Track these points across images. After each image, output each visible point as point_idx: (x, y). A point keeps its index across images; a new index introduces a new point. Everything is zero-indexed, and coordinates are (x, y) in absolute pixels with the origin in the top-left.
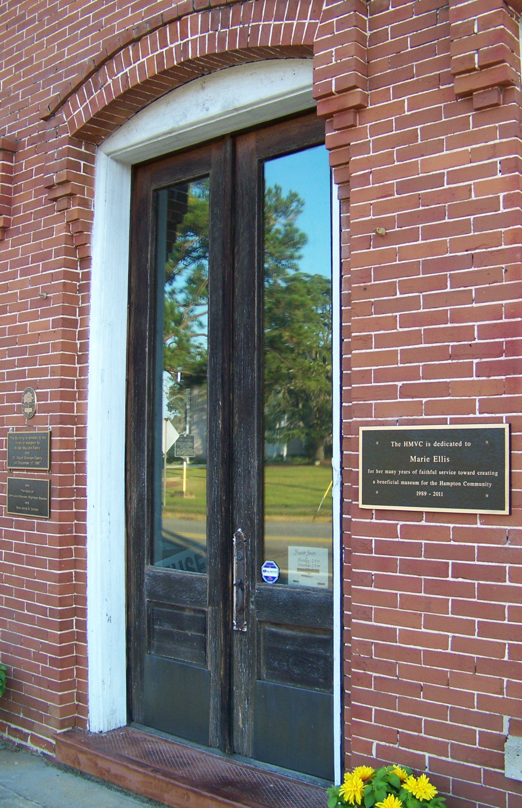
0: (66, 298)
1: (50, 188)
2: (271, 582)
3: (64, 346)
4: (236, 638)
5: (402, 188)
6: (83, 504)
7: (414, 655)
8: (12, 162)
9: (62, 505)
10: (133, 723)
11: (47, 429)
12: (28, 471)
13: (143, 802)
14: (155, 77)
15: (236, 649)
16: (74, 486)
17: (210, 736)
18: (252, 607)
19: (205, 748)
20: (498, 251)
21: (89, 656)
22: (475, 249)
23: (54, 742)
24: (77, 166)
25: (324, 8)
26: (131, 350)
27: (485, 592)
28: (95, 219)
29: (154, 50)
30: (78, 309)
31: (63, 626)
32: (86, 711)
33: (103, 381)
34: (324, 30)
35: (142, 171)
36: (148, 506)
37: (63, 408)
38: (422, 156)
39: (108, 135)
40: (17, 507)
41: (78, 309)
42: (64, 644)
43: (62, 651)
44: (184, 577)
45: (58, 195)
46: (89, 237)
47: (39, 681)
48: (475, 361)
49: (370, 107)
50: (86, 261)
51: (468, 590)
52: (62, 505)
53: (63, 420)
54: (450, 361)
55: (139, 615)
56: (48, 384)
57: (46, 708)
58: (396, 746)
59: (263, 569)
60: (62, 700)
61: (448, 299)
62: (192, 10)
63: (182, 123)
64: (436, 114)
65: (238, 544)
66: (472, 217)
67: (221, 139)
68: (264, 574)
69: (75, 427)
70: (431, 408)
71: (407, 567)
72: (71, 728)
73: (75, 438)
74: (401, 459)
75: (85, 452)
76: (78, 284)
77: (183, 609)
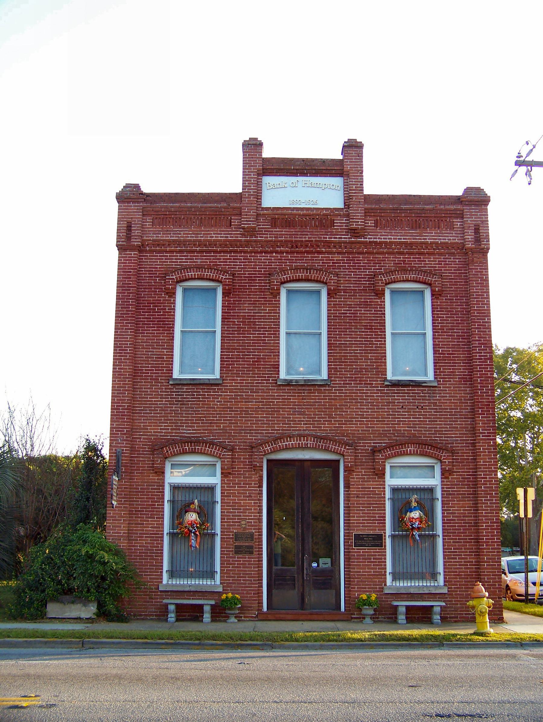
7: (365, 575)
26: (338, 553)
27: (379, 562)
34: (347, 452)
51: (376, 562)
61: (372, 510)
64: (369, 475)
70: (368, 530)
71: (363, 559)
74: (362, 539)
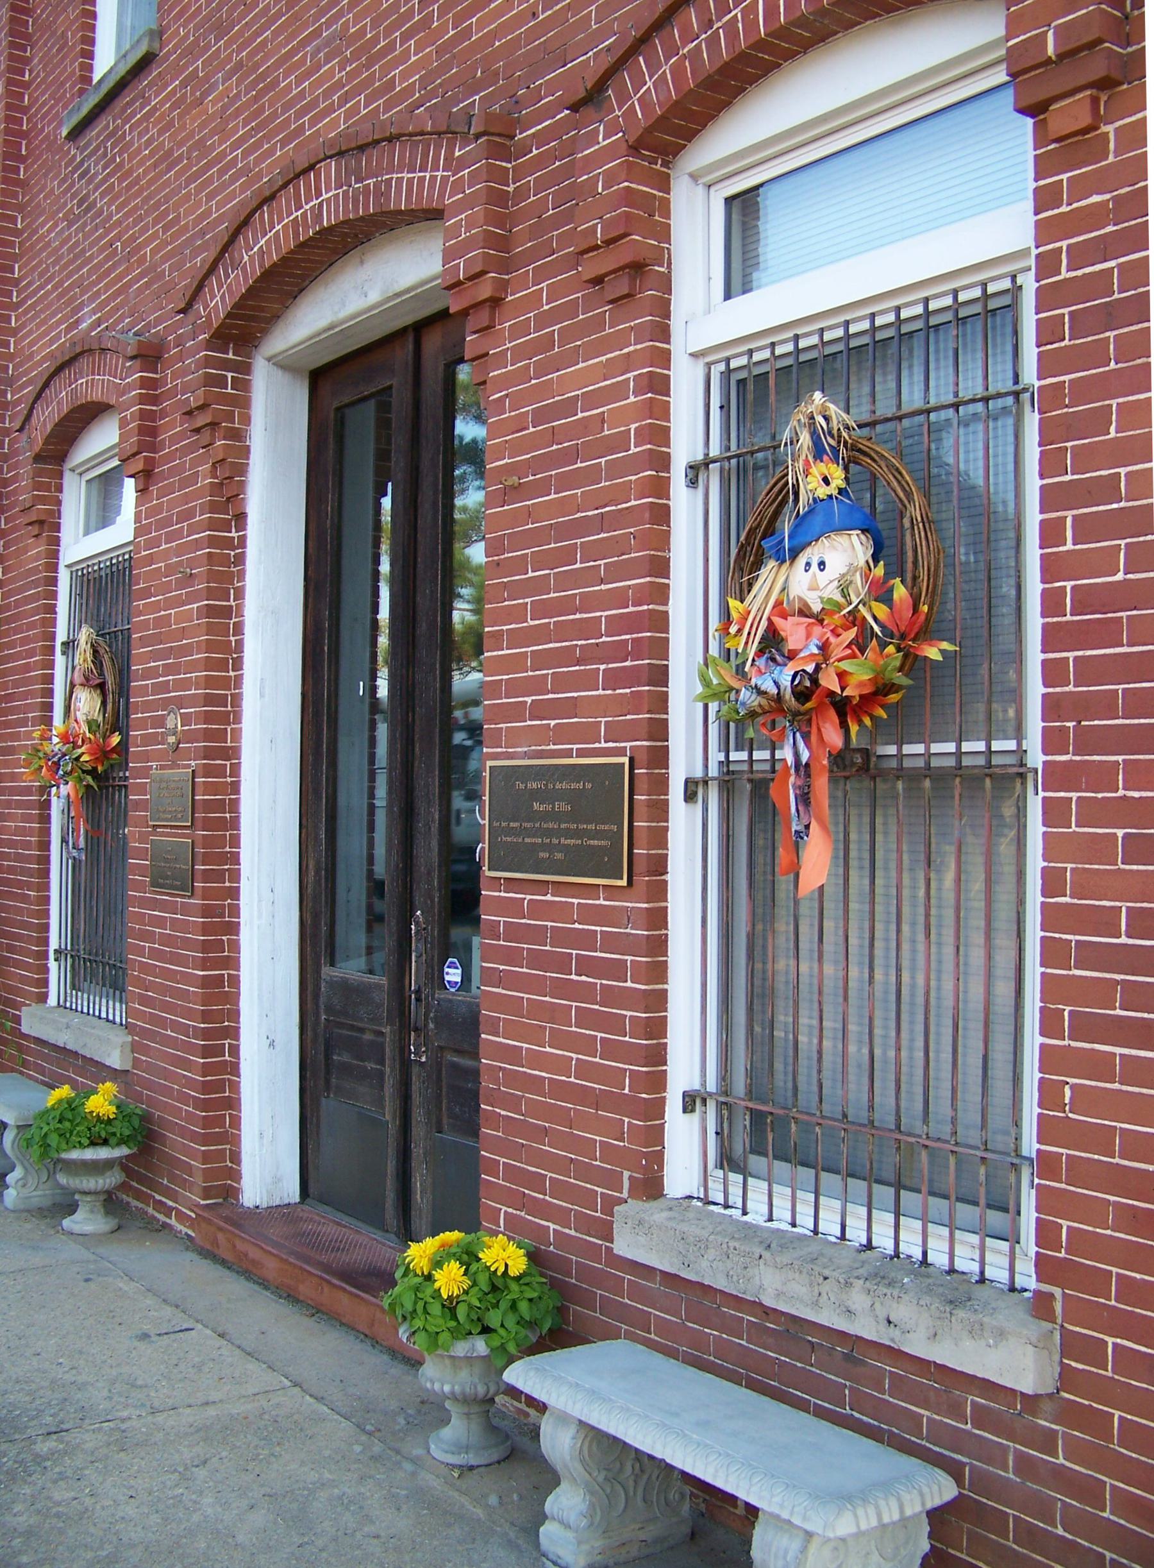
0: (211, 576)
1: (189, 413)
2: (453, 990)
3: (210, 646)
4: (415, 1070)
5: (540, 417)
6: (236, 876)
8: (157, 373)
9: (207, 876)
10: (308, 1200)
11: (189, 766)
12: (172, 827)
13: (280, 1297)
14: (292, 252)
15: (416, 1086)
16: (228, 849)
17: (387, 1216)
18: (431, 1026)
19: (381, 1234)
20: (627, 508)
21: (243, 1096)
22: (605, 506)
23: (193, 1215)
24: (221, 382)
25: (457, 154)
28: (252, 456)
29: (289, 214)
30: (232, 591)
31: (206, 1052)
32: (236, 1175)
33: (262, 695)
35: (331, 380)
36: (326, 878)
37: (208, 735)
38: (558, 370)
39: (265, 332)
40: (161, 881)
41: (232, 591)
42: (209, 1078)
43: (206, 1087)
44: (362, 982)
45: (199, 425)
46: (242, 484)
47: (183, 1132)
48: (602, 667)
49: (510, 298)
50: (241, 519)
52: (207, 876)
53: (208, 754)
54: (577, 668)
55: (315, 1040)
56: (192, 701)
57: (189, 1169)
58: (523, 1214)
59: (446, 970)
60: (206, 1157)
62: (322, 156)
63: (342, 314)
64: (571, 309)
65: (417, 932)
66: (603, 460)
67: (402, 332)
68: (447, 978)
69: (228, 763)
72: (221, 1200)
73: (229, 780)
75: (239, 799)
76: (232, 553)
77: (362, 1030)
